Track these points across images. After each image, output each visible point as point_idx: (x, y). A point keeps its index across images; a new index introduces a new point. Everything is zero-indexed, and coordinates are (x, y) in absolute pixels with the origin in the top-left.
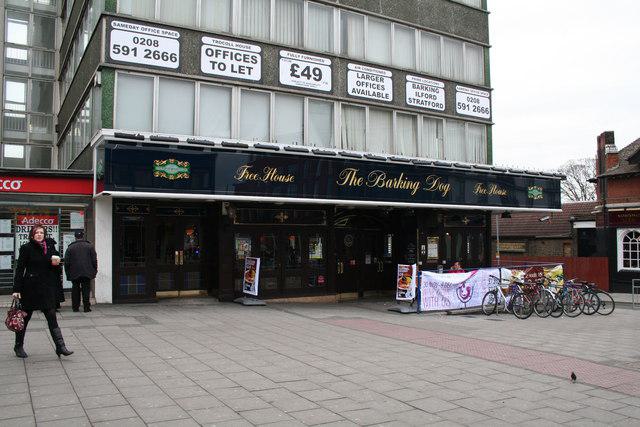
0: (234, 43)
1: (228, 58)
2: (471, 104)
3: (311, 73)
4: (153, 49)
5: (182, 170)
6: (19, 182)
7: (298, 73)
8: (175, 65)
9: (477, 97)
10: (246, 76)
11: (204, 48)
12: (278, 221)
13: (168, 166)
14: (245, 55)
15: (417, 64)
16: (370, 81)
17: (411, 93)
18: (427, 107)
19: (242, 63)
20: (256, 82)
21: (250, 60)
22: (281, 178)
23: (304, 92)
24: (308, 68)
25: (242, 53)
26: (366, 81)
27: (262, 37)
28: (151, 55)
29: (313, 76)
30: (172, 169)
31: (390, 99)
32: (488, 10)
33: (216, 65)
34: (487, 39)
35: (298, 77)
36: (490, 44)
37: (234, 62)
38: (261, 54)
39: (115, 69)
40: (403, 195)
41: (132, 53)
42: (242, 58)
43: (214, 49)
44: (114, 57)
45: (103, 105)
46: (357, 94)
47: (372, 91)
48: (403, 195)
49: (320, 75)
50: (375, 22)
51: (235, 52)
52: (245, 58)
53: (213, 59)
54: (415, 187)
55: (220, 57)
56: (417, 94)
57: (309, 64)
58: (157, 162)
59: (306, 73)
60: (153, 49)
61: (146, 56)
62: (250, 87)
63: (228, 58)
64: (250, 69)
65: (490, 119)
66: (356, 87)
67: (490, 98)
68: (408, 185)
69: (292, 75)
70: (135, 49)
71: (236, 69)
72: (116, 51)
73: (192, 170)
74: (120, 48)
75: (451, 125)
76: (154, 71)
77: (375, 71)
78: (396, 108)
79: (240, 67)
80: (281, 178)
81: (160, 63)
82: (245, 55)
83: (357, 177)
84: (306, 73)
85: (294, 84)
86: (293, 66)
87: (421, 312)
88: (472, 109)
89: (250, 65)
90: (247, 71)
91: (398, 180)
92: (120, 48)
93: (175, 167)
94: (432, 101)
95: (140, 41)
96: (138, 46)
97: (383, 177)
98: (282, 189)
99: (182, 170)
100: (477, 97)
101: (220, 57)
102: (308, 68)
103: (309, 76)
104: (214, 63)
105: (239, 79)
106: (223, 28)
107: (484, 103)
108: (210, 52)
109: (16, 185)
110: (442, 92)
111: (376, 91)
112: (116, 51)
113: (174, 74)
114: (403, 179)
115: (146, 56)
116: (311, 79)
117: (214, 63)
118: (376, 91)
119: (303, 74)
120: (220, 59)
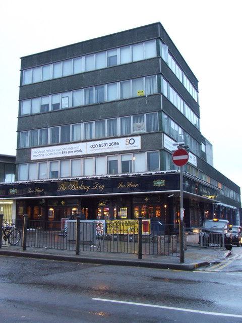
22: (134, 186)
30: (159, 183)
68: (85, 188)
80: (134, 186)
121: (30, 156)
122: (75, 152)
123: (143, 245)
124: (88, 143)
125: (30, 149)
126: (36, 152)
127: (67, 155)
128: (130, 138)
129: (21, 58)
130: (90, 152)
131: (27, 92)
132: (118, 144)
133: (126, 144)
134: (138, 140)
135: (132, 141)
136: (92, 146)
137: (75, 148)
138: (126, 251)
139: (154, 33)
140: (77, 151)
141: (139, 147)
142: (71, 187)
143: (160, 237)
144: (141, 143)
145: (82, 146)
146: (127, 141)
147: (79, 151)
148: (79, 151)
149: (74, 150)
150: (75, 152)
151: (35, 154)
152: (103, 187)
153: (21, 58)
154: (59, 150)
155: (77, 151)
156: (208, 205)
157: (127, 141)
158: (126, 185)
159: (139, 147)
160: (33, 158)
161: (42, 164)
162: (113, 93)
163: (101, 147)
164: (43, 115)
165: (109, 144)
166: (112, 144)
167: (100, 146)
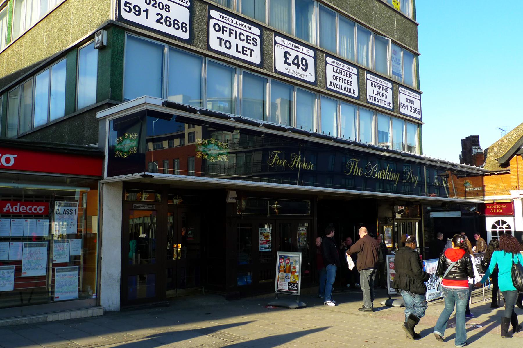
0: (239, 22)
1: (233, 36)
2: (409, 105)
3: (300, 63)
4: (165, 14)
6: (12, 157)
7: (290, 61)
8: (186, 36)
9: (412, 99)
10: (248, 58)
11: (212, 22)
14: (247, 36)
16: (342, 76)
17: (370, 90)
18: (381, 104)
19: (245, 44)
20: (256, 65)
21: (252, 42)
24: (297, 57)
25: (245, 33)
26: (340, 76)
28: (163, 21)
29: (301, 66)
31: (356, 95)
32: (419, 52)
33: (223, 42)
34: (417, 48)
35: (290, 65)
36: (420, 52)
37: (238, 41)
38: (261, 36)
41: (143, 14)
42: (245, 38)
43: (221, 24)
44: (126, 16)
45: (112, 70)
46: (333, 88)
47: (344, 85)
49: (306, 65)
50: (347, 23)
51: (239, 31)
52: (247, 39)
53: (220, 35)
55: (226, 33)
56: (374, 91)
57: (298, 54)
59: (296, 62)
60: (165, 14)
61: (158, 21)
63: (233, 36)
64: (252, 50)
65: (421, 120)
66: (333, 81)
67: (420, 100)
69: (286, 62)
70: (147, 11)
71: (240, 49)
72: (128, 9)
74: (132, 7)
77: (345, 67)
78: (359, 103)
79: (243, 47)
81: (171, 31)
82: (247, 36)
83: (359, 167)
84: (296, 62)
85: (286, 72)
86: (286, 53)
87: (372, 302)
88: (409, 109)
89: (252, 47)
90: (249, 52)
91: (385, 171)
92: (132, 7)
94: (384, 99)
96: (150, 7)
98: (305, 177)
100: (412, 99)
101: (226, 33)
102: (297, 57)
103: (298, 66)
104: (221, 39)
105: (244, 61)
107: (417, 105)
108: (217, 28)
109: (8, 160)
110: (390, 91)
111: (347, 86)
112: (128, 9)
114: (389, 171)
115: (158, 21)
116: (300, 68)
117: (221, 39)
118: (347, 86)
119: (293, 63)
120: (226, 36)
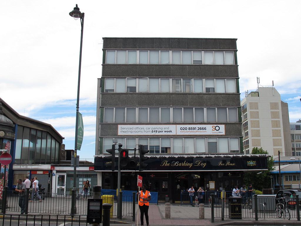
5: (254, 163)
12: (151, 177)
13: (251, 163)
15: (228, 120)
22: (231, 164)
23: (124, 137)
27: (224, 121)
30: (251, 163)
39: (103, 138)
40: (187, 168)
48: (187, 168)
54: (191, 165)
58: (248, 162)
62: (141, 137)
68: (188, 164)
73: (256, 163)
75: (232, 139)
76: (182, 137)
80: (231, 164)
83: (168, 163)
93: (252, 163)
95: (183, 129)
97: (177, 163)
99: (254, 163)
106: (122, 122)
113: (224, 136)
114: (186, 163)
121: (118, 132)
122: (165, 132)
123: (215, 209)
124: (178, 126)
125: (116, 125)
126: (123, 129)
127: (157, 134)
128: (216, 125)
129: (103, 38)
130: (179, 133)
131: (109, 71)
132: (205, 129)
133: (213, 130)
134: (222, 127)
135: (217, 128)
136: (181, 129)
137: (165, 128)
138: (247, 217)
139: (230, 45)
140: (167, 132)
141: (224, 133)
142: (174, 163)
143: (63, 190)
144: (225, 131)
145: (172, 127)
146: (214, 127)
147: (169, 132)
148: (169, 132)
149: (165, 130)
150: (165, 132)
151: (122, 130)
152: (205, 165)
153: (103, 38)
154: (149, 129)
155: (167, 132)
156: (138, 165)
157: (214, 127)
158: (35, 143)
159: (224, 133)
160: (120, 133)
161: (106, 140)
162: (198, 86)
163: (182, 130)
164: (130, 95)
165: (197, 129)
166: (200, 129)
167: (189, 129)
